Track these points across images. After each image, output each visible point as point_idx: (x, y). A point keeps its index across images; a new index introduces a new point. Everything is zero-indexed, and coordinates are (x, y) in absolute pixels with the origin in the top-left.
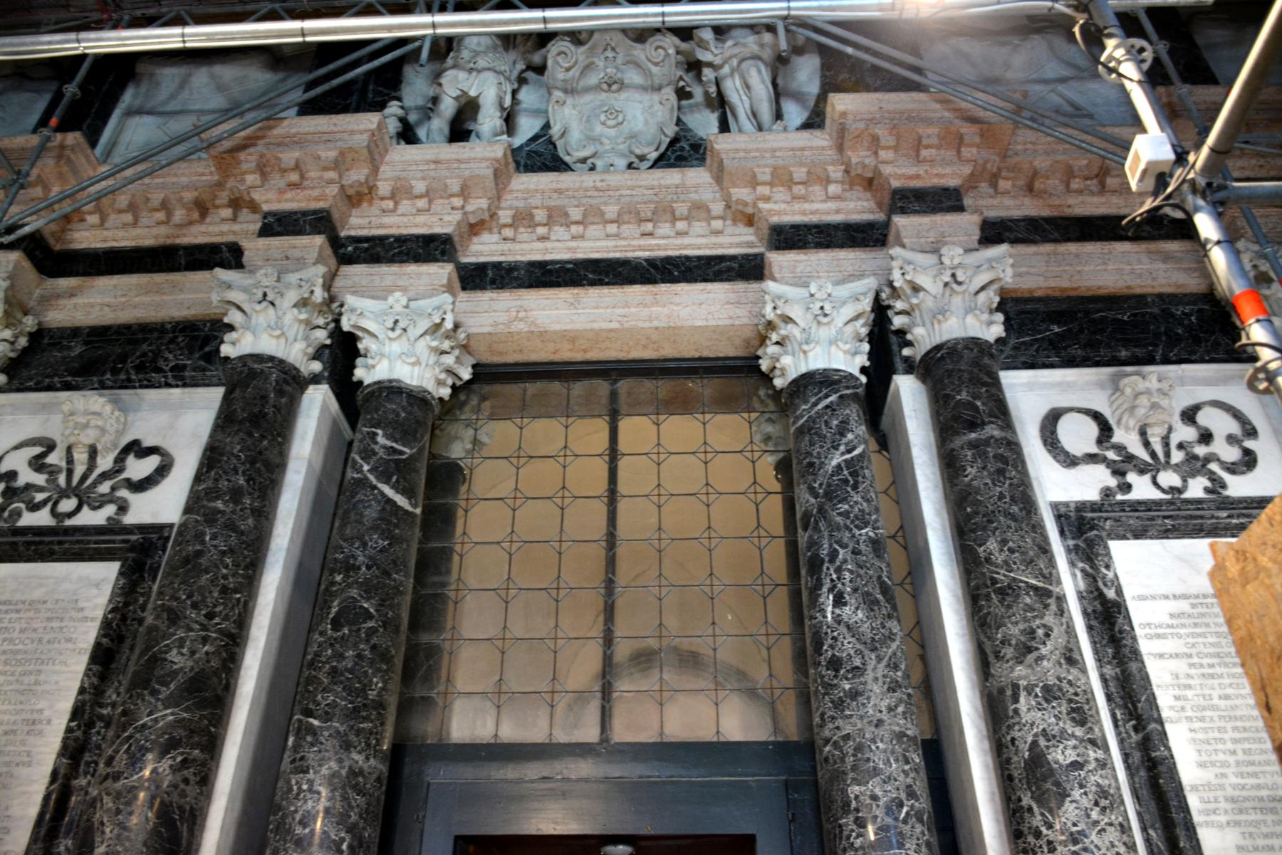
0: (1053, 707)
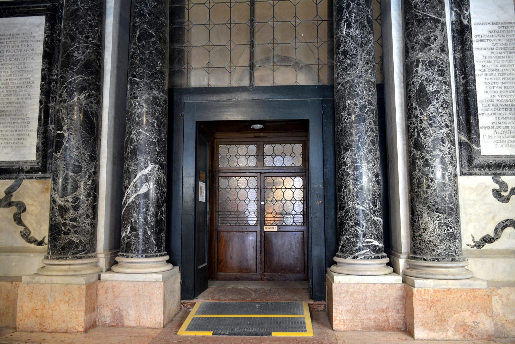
0: (432, 69)
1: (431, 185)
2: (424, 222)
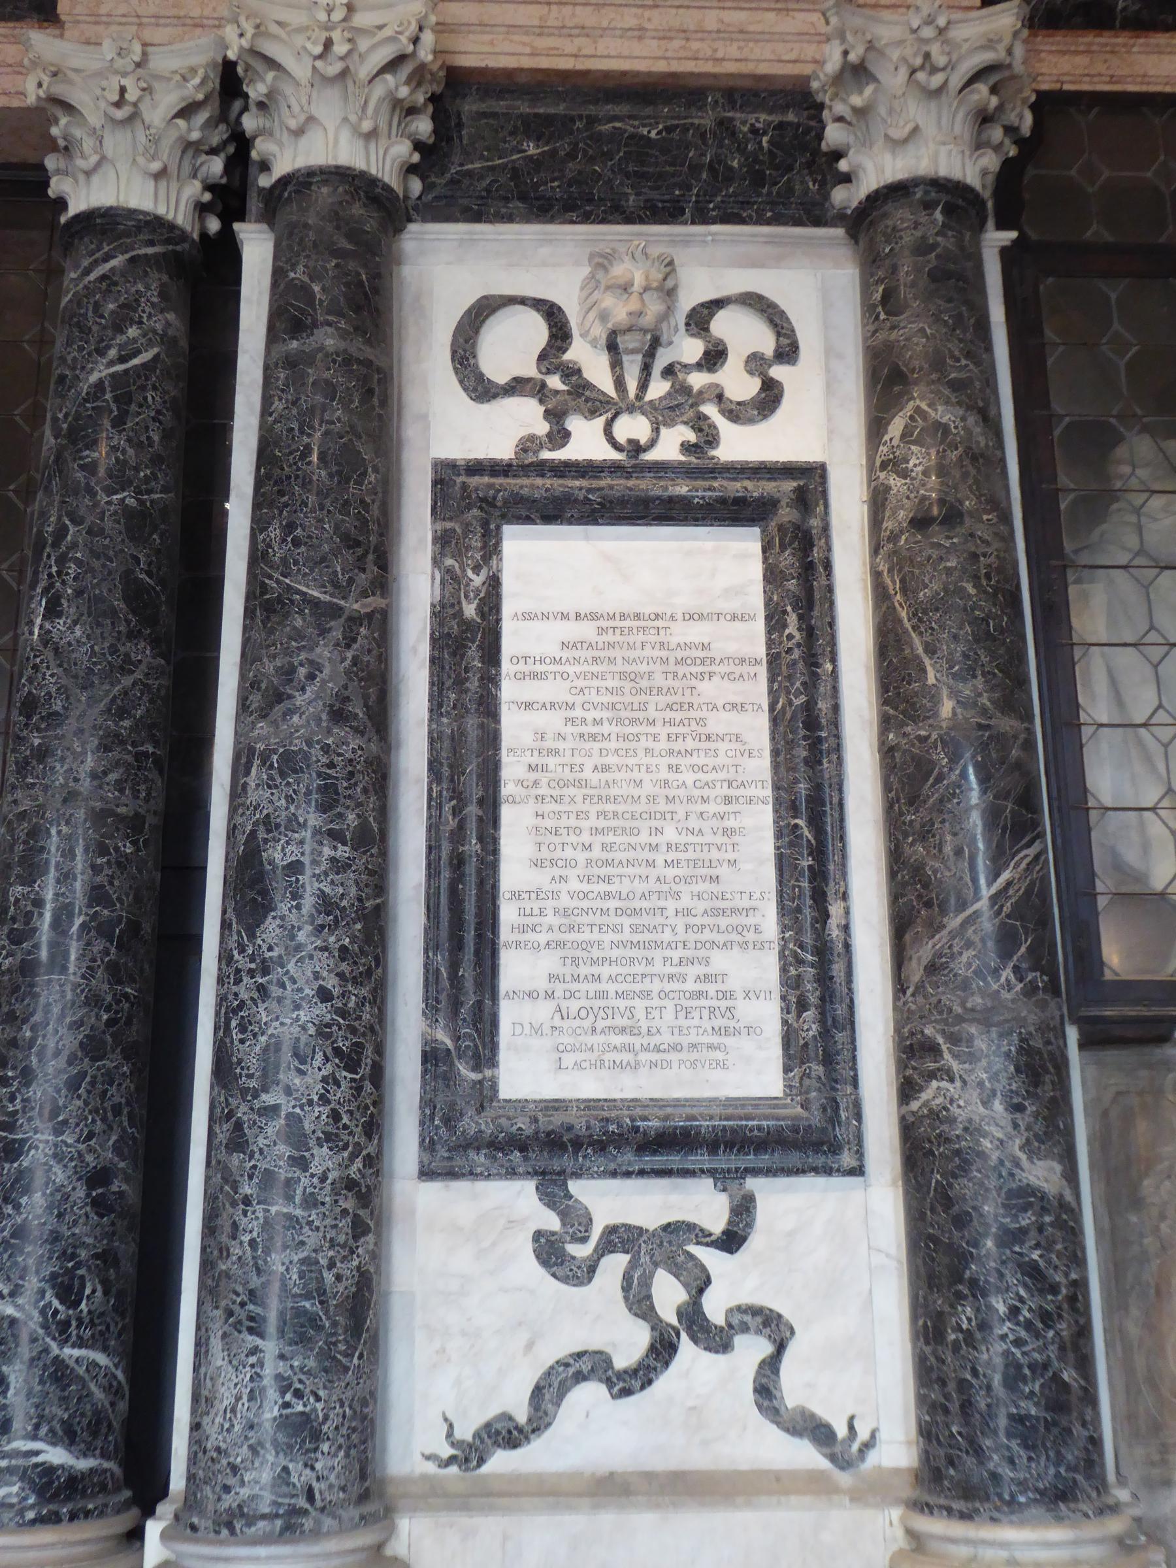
0: (288, 784)
1: (243, 1222)
2: (211, 1369)
